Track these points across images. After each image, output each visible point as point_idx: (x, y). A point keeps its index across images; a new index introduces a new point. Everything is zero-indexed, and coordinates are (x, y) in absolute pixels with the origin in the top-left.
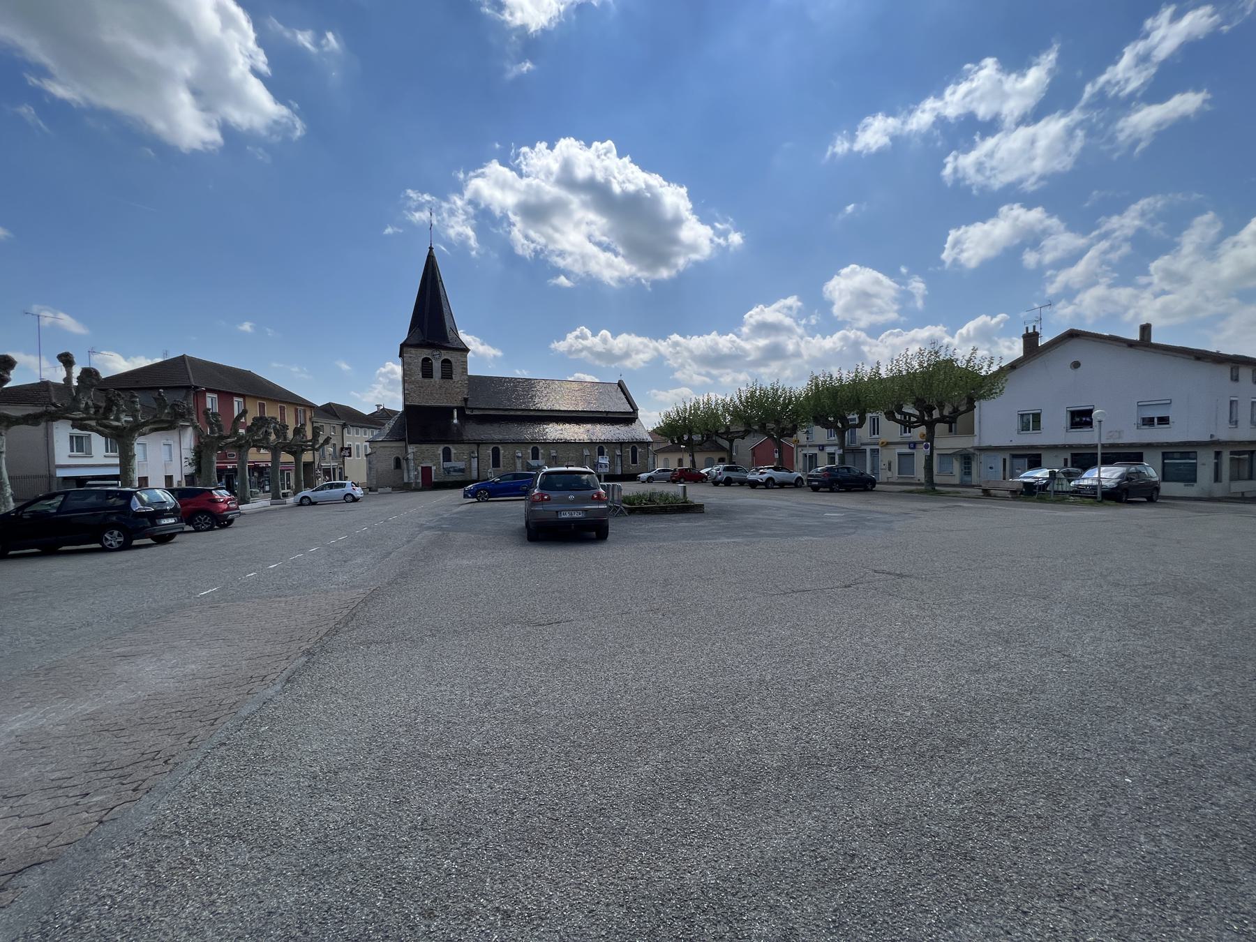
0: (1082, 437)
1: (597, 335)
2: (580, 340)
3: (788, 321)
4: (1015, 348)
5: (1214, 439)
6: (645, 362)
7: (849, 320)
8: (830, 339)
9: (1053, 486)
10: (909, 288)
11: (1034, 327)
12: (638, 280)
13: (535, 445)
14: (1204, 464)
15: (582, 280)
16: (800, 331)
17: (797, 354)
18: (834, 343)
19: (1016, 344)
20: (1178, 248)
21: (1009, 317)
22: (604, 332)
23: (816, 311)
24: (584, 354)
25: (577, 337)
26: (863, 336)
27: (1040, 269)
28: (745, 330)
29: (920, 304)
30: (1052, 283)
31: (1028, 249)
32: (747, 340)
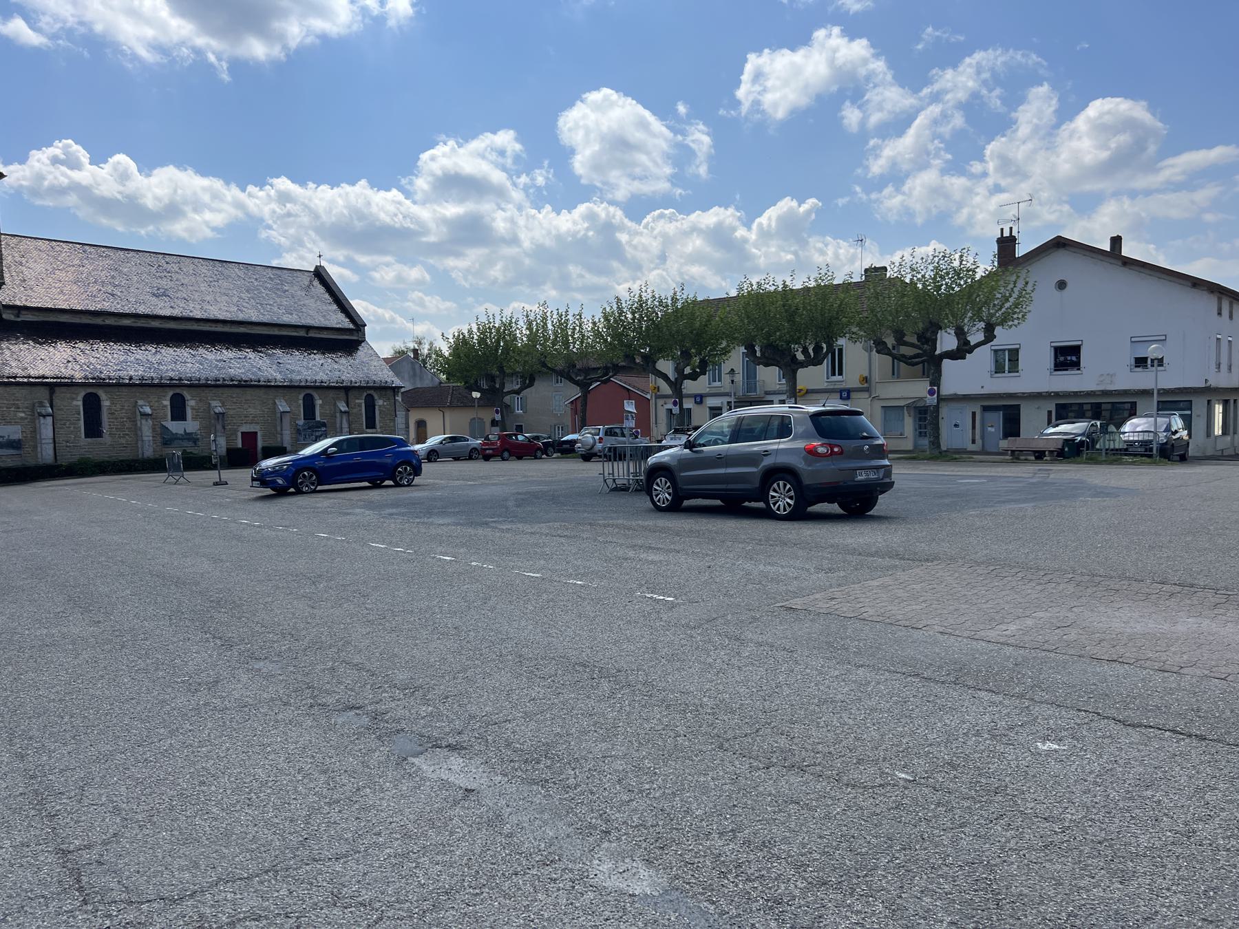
0: (1068, 382)
1: (106, 162)
2: (63, 168)
3: (497, 177)
4: (828, 252)
5: (1208, 384)
6: (214, 229)
7: (599, 185)
8: (568, 216)
9: (1104, 442)
10: (688, 140)
11: (1011, 228)
12: (198, 51)
13: (178, 391)
14: (1198, 416)
15: (69, 33)
16: (517, 195)
17: (514, 241)
18: (575, 223)
19: (829, 247)
20: (1014, 127)
21: (820, 204)
22: (121, 158)
23: (546, 163)
24: (72, 199)
25: (55, 161)
26: (618, 214)
27: (864, 134)
28: (422, 184)
29: (703, 170)
30: (877, 157)
31: (848, 103)
32: (424, 203)
